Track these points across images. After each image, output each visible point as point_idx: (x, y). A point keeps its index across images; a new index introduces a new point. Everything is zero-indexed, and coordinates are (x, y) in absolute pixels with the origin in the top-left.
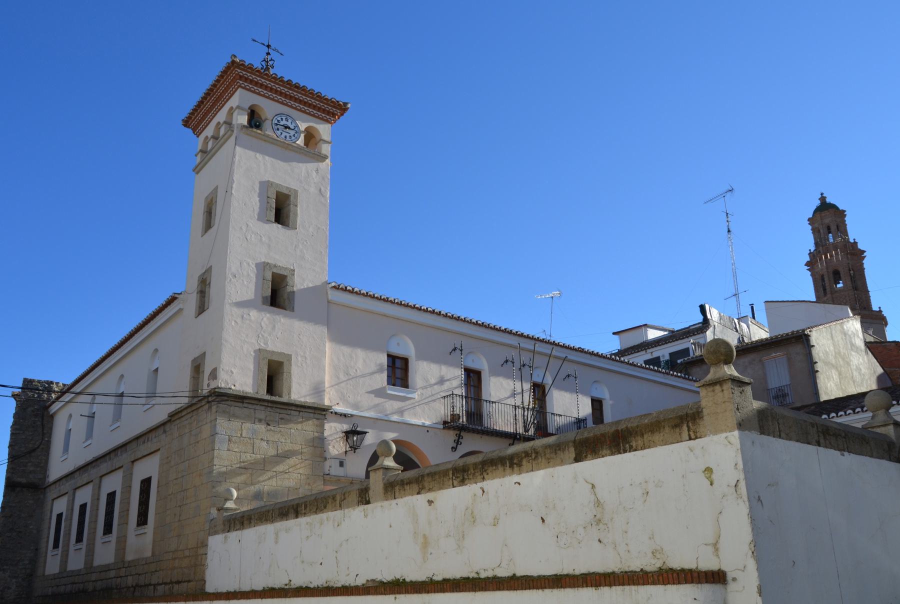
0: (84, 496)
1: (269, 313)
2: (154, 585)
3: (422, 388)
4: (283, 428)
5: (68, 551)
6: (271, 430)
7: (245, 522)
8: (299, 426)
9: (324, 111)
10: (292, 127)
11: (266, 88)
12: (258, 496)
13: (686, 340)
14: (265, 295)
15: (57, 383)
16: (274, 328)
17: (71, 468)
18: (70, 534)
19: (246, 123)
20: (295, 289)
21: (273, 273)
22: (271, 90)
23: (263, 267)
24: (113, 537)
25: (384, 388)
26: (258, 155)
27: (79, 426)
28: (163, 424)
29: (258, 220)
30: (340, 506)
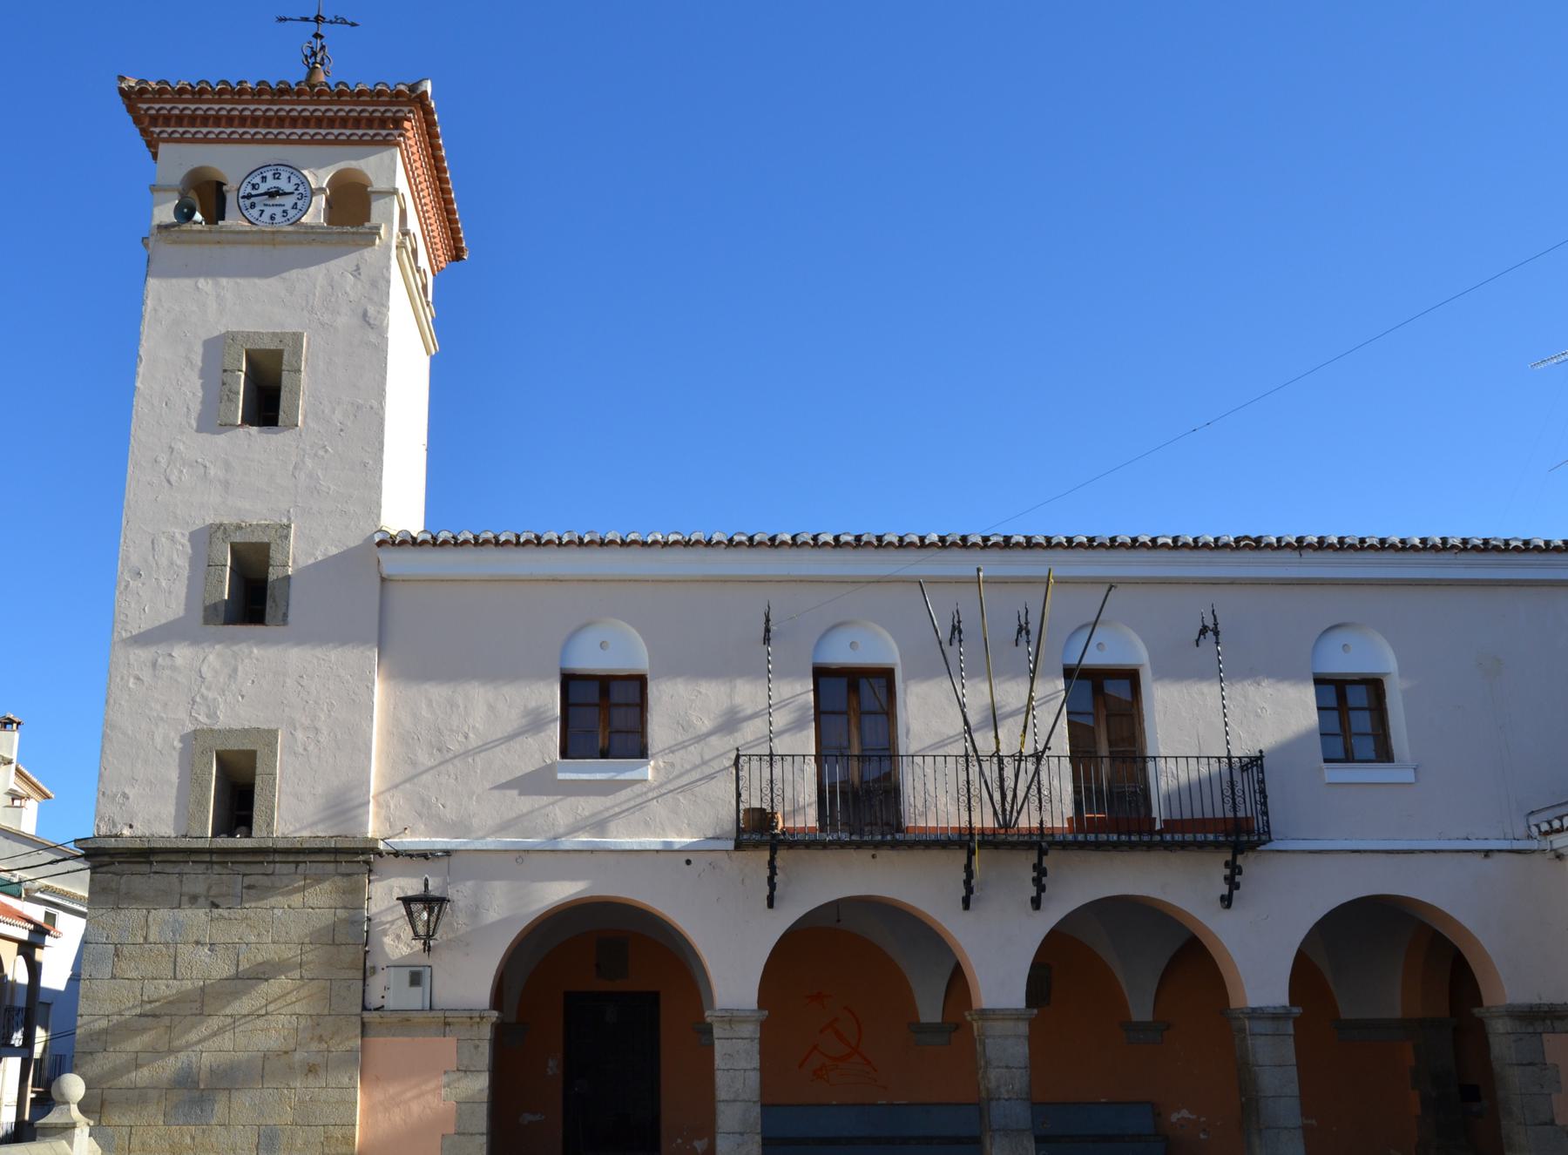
3: (672, 750)
4: (255, 910)
8: (296, 900)
9: (370, 123)
10: (289, 188)
25: (550, 769)
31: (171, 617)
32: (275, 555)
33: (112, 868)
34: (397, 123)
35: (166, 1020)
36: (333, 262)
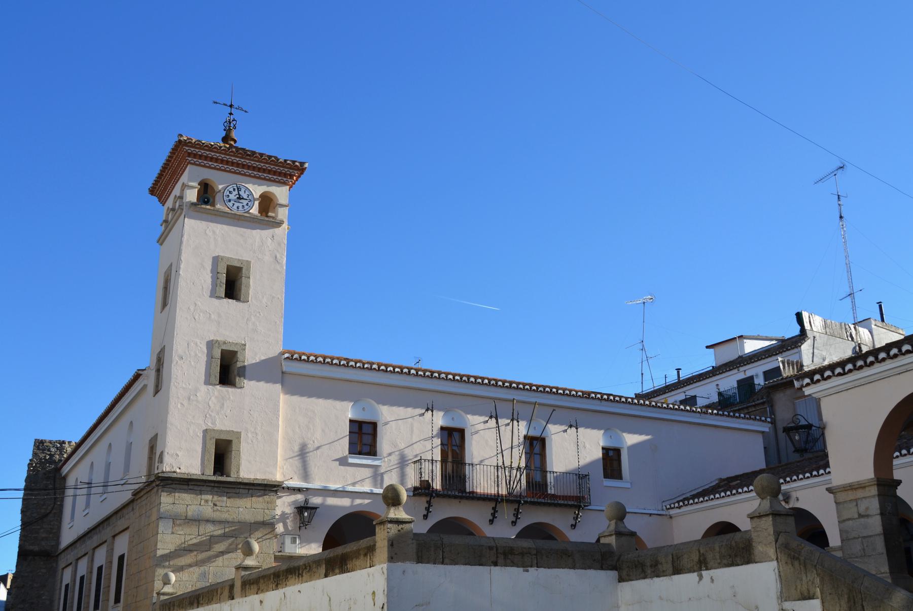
6: (218, 510)
9: (280, 174)
10: (245, 197)
11: (217, 160)
13: (774, 358)
15: (70, 442)
22: (222, 161)
28: (131, 502)
32: (239, 355)
34: (291, 176)
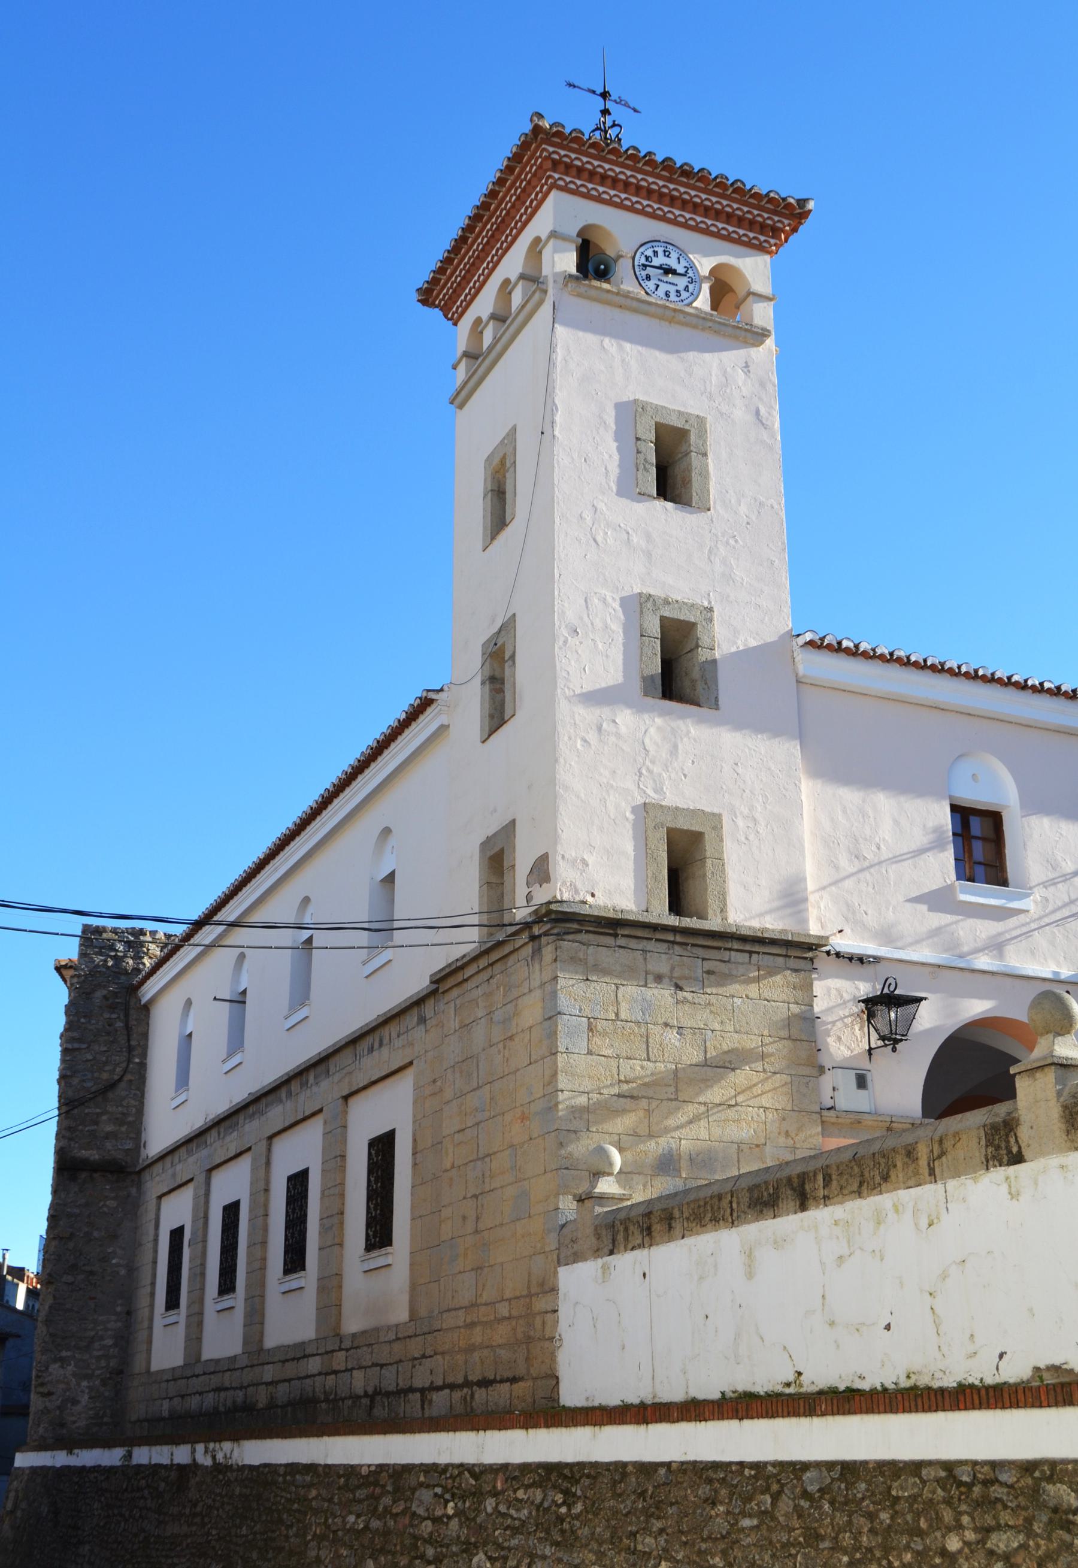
0: (232, 1184)
1: (663, 714)
2: (422, 1391)
3: (1045, 884)
4: (715, 994)
5: (201, 1314)
6: (685, 1001)
7: (657, 1227)
8: (753, 990)
9: (752, 225)
10: (681, 270)
11: (614, 182)
12: (667, 1164)
14: (648, 672)
16: (674, 751)
17: (198, 1122)
18: (203, 1275)
19: (573, 270)
20: (717, 655)
21: (663, 619)
22: (626, 186)
23: (638, 604)
24: (310, 1277)
25: (950, 888)
26: (607, 340)
27: (210, 1025)
28: (419, 1002)
29: (620, 493)
30: (932, 1172)
31: (611, 683)
33: (578, 937)
35: (644, 1103)
36: (725, 353)
